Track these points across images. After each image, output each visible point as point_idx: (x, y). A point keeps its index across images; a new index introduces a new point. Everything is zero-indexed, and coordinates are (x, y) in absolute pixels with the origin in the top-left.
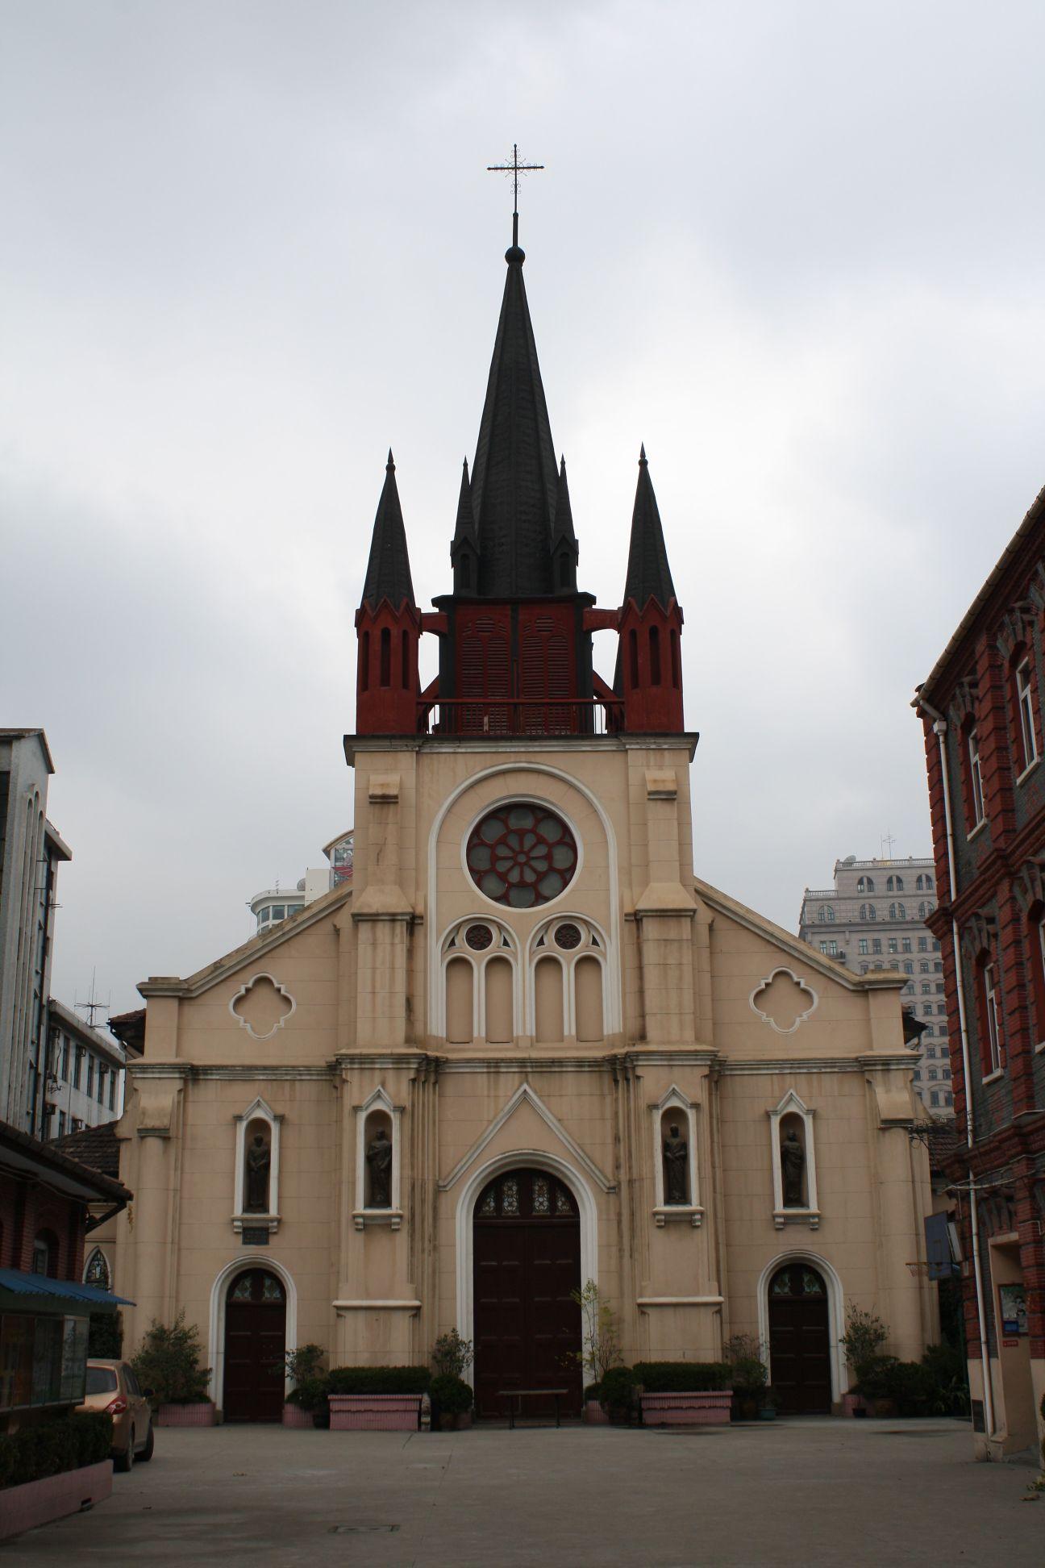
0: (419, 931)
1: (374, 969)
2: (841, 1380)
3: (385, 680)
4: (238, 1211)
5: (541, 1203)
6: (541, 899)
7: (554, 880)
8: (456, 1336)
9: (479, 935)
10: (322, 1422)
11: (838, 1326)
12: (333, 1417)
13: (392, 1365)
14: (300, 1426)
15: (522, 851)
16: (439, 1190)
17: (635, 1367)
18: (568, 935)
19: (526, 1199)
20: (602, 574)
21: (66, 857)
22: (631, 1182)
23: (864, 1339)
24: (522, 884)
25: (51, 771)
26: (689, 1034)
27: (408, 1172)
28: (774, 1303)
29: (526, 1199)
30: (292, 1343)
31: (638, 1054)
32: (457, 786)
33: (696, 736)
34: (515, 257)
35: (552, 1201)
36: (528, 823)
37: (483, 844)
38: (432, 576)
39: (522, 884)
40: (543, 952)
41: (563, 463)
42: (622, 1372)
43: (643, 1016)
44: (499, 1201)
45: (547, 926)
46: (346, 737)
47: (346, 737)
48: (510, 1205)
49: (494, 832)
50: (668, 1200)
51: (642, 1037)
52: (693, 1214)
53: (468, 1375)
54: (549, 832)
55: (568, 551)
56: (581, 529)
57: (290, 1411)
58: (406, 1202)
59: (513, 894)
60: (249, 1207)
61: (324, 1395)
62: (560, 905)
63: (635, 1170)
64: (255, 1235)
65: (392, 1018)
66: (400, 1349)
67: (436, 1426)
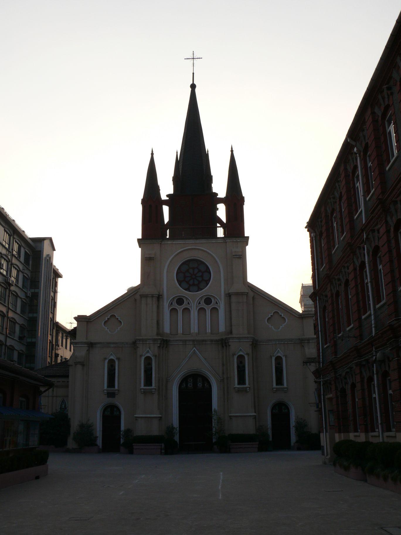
2: (293, 438)
4: (106, 387)
5: (200, 385)
6: (200, 289)
10: (131, 452)
18: (208, 301)
20: (220, 187)
25: (54, 250)
28: (273, 415)
30: (123, 428)
31: (229, 338)
34: (193, 86)
38: (166, 188)
48: (190, 385)
51: (231, 333)
52: (246, 388)
53: (177, 438)
60: (109, 386)
62: (205, 292)
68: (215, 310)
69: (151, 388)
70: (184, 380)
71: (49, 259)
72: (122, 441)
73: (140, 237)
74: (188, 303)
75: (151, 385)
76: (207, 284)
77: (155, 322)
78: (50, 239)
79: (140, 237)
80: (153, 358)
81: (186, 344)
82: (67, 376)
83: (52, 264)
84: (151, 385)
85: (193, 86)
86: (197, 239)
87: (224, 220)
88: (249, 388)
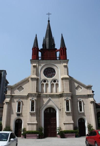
0: (38, 80)
1: (33, 84)
2: (87, 132)
3: (35, 55)
4: (17, 112)
5: (52, 111)
6: (52, 77)
7: (53, 75)
8: (42, 127)
9: (45, 81)
10: (25, 138)
11: (86, 125)
12: (26, 137)
13: (34, 131)
14: (22, 138)
15: (50, 72)
16: (40, 108)
17: (64, 131)
18: (55, 81)
19: (50, 111)
20: (58, 46)
21: (9, 83)
22: (62, 109)
23: (90, 127)
24: (50, 76)
25: (6, 74)
26: (69, 91)
27: (36, 107)
28: (79, 123)
29: (50, 111)
30: (22, 128)
31: (63, 93)
32: (42, 66)
33: (69, 60)
34: (49, 21)
35: (53, 111)
36: (50, 69)
37: (45, 71)
38: (40, 47)
39: (50, 76)
40: (52, 83)
41: (54, 38)
42: (62, 131)
43: (63, 90)
44: (47, 111)
45: (52, 80)
46: (30, 60)
47: (30, 60)
48: (48, 111)
49: (46, 70)
50: (67, 111)
51: (63, 92)
52: (70, 112)
53: (43, 132)
54: (52, 70)
55: (54, 45)
56: (55, 43)
57: (22, 136)
58: (36, 111)
59: (49, 77)
60: (18, 111)
61: (26, 134)
62: (54, 78)
63: (85, 86)
64: (18, 115)
65: (35, 90)
66: (34, 128)
67: (39, 138)
68: (57, 85)
69: (34, 112)
70: (46, 110)
71: (5, 77)
72: (22, 133)
73: (31, 59)
74: (48, 82)
75: (69, 110)
76: (54, 76)
77: (36, 87)
78: (5, 71)
79: (31, 59)
80: (35, 101)
81: (47, 96)
82: (3, 108)
83: (5, 78)
84: (20, 112)
85: (49, 21)
86: (51, 60)
87: (32, 98)
88: (71, 112)
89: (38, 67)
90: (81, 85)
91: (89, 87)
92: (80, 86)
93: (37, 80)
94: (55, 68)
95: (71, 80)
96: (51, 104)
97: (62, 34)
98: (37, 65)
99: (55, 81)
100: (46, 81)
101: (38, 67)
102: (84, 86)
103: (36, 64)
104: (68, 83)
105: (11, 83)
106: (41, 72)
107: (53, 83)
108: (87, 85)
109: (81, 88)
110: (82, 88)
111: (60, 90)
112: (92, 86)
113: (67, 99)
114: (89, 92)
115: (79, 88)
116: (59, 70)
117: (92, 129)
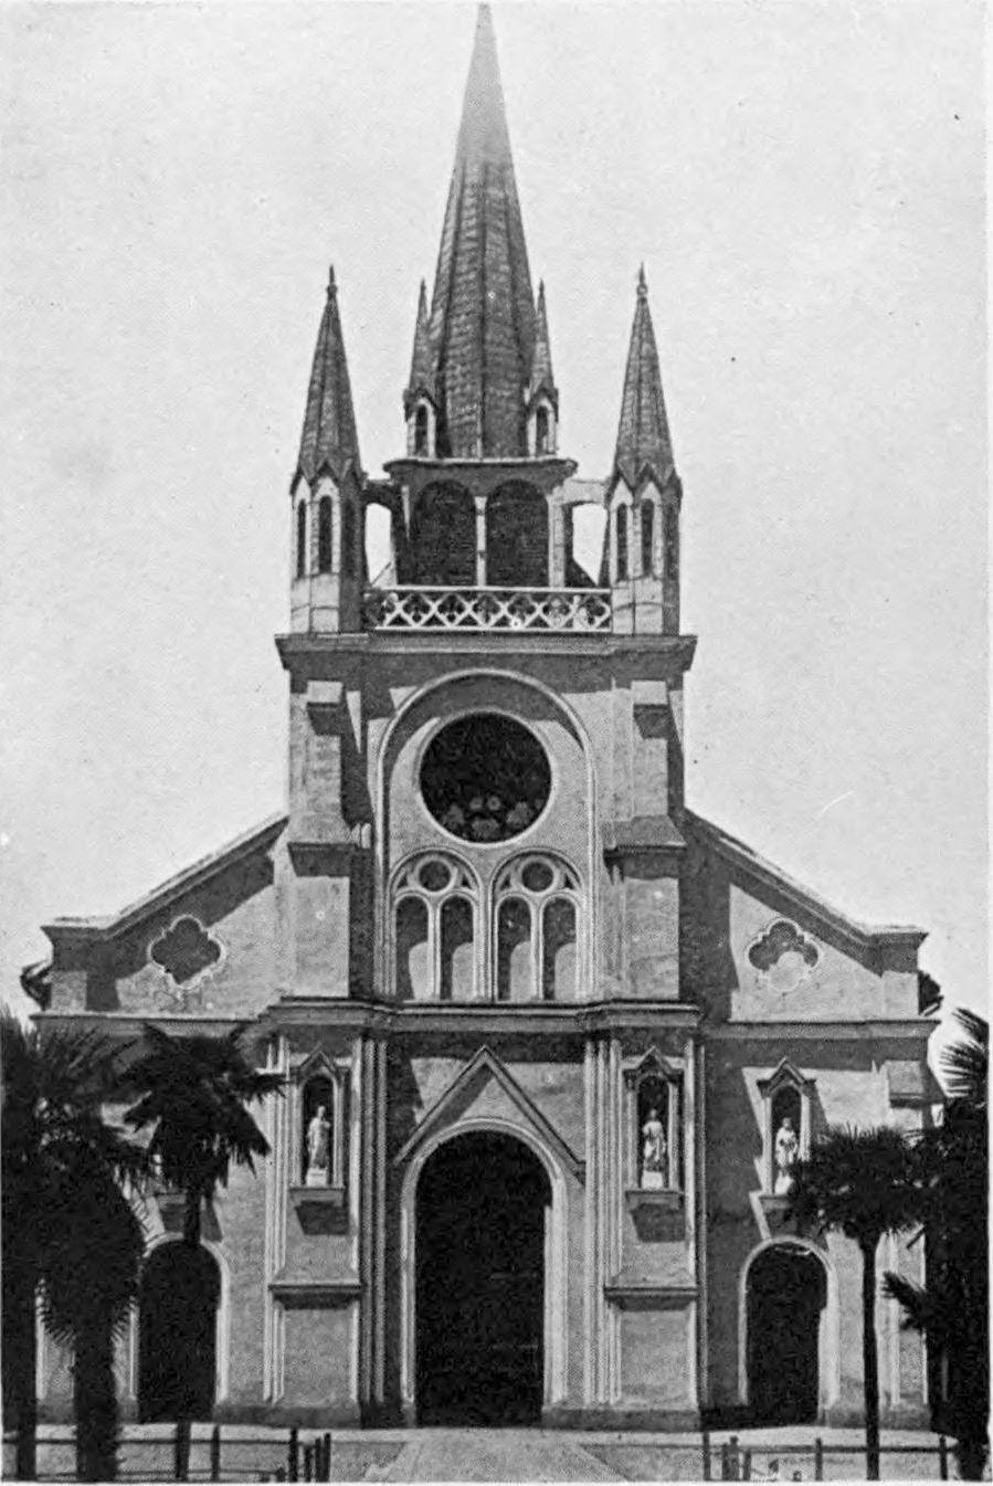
3: (324, 564)
20: (586, 433)
38: (383, 439)
68: (560, 921)
89: (364, 727)
90: (802, 920)
91: (888, 952)
92: (799, 931)
93: (357, 866)
94: (545, 731)
95: (703, 865)
96: (491, 1111)
97: (647, 274)
98: (354, 699)
99: (536, 876)
100: (447, 876)
101: (364, 727)
102: (830, 929)
103: (338, 686)
104: (664, 893)
105: (191, 1467)
106: (397, 766)
107: (518, 889)
108: (871, 918)
109: (811, 956)
110: (821, 954)
111: (582, 980)
112: (923, 936)
113: (643, 1068)
114: (893, 997)
115: (790, 959)
116: (354, 1396)
117: (921, 1334)
